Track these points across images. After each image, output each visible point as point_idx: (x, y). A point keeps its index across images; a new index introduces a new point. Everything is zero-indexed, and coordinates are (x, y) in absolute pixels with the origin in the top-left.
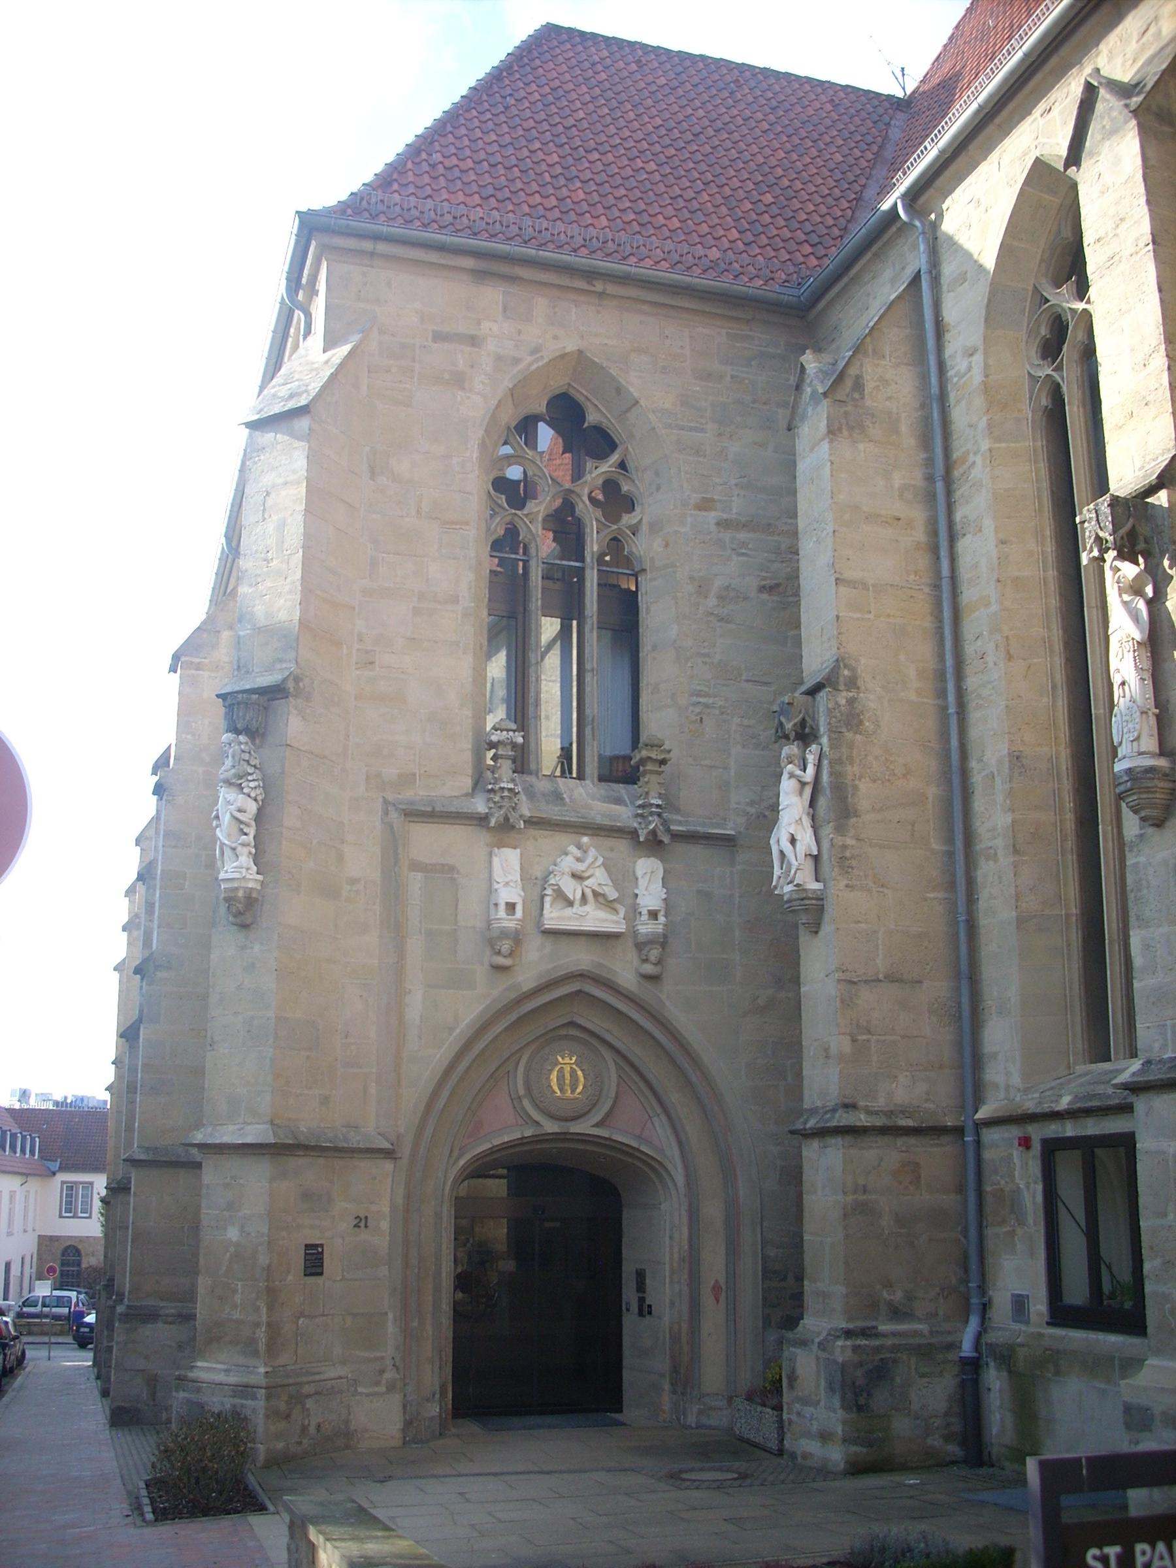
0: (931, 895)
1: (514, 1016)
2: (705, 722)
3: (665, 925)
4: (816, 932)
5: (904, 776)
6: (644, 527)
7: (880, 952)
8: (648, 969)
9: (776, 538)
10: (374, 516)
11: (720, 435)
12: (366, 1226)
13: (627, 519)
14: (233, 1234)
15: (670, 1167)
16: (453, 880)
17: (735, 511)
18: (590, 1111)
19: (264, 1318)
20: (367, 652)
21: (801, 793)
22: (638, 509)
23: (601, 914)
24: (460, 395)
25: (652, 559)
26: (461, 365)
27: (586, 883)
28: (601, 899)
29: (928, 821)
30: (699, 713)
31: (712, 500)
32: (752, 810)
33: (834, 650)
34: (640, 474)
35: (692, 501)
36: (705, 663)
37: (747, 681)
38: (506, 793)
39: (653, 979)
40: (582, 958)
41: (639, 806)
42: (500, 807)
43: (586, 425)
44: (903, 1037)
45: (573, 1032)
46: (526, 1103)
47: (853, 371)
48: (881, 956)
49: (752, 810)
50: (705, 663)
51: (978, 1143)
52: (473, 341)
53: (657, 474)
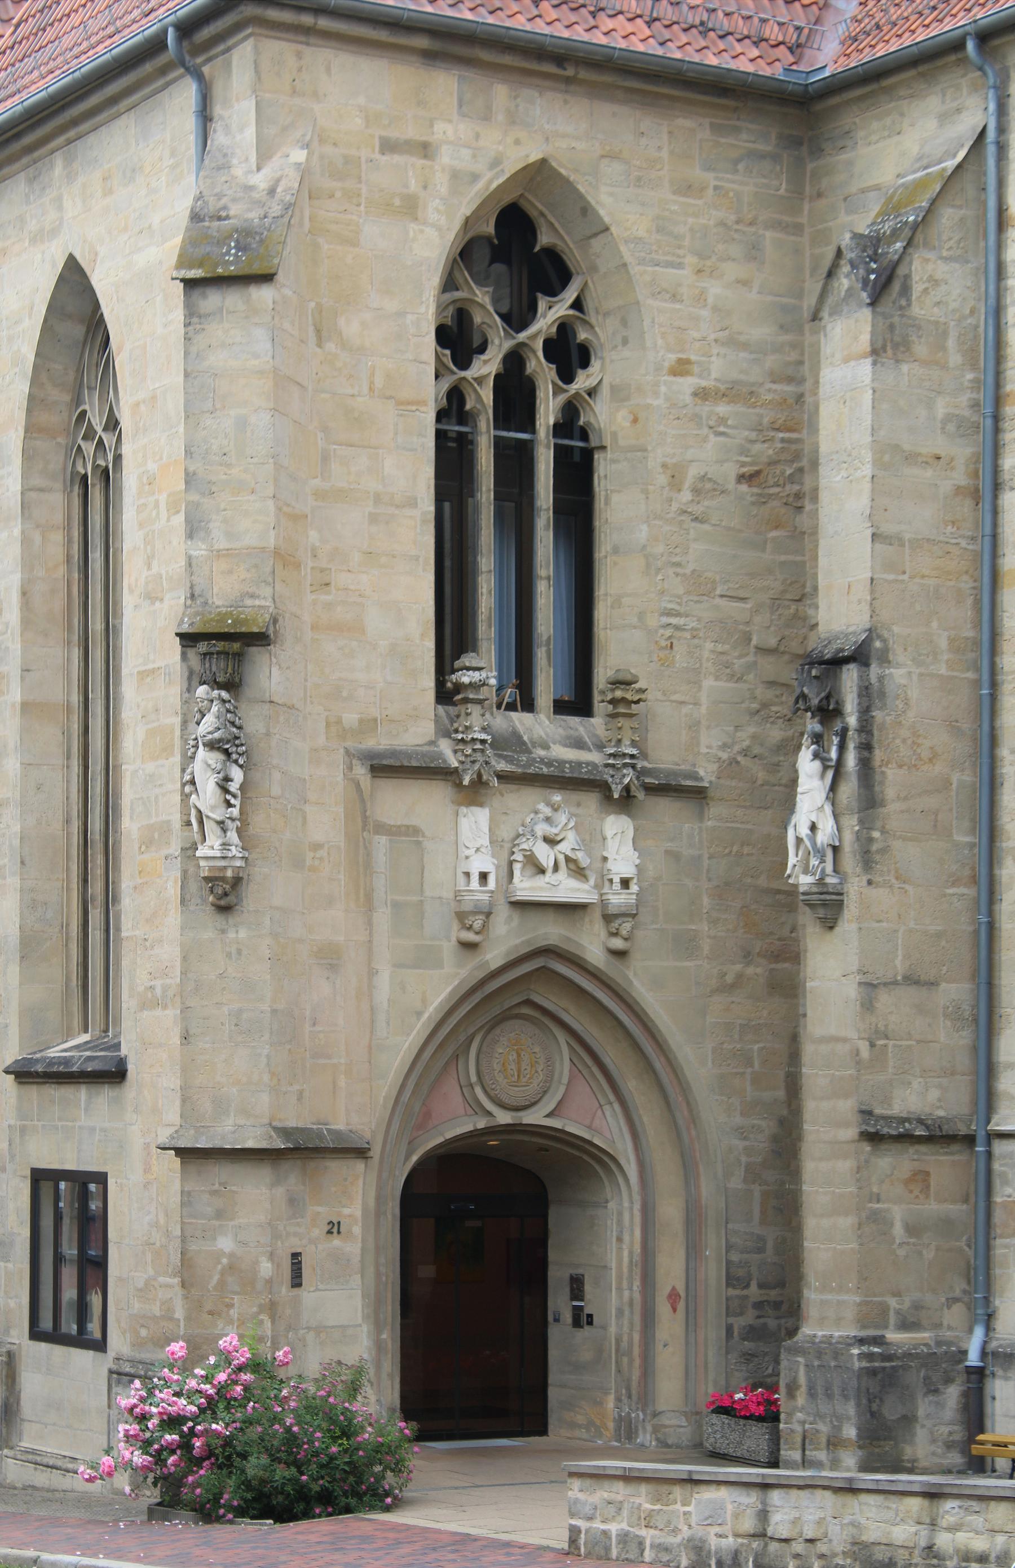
0: (950, 891)
1: (478, 997)
2: (675, 648)
3: (637, 895)
4: (831, 928)
5: (930, 760)
6: (605, 391)
7: (900, 952)
8: (618, 943)
9: (757, 410)
10: (323, 395)
11: (699, 271)
12: (339, 1232)
13: (583, 381)
14: (225, 1244)
15: (622, 1161)
16: (419, 843)
17: (714, 376)
18: (541, 1098)
19: (269, 1333)
20: (322, 570)
21: (822, 776)
22: (595, 365)
23: (573, 883)
24: (413, 226)
25: (614, 435)
26: (414, 186)
27: (560, 847)
28: (572, 866)
29: (951, 810)
30: (670, 637)
31: (688, 362)
32: (725, 756)
33: (866, 617)
34: (600, 318)
35: (666, 364)
36: (677, 575)
37: (722, 596)
38: (478, 746)
39: (620, 954)
40: (551, 931)
41: (611, 755)
42: (473, 762)
43: (537, 249)
44: (918, 1042)
45: (526, 1010)
46: (478, 1091)
47: (901, 271)
48: (900, 958)
49: (725, 756)
50: (677, 575)
51: (989, 1155)
52: (425, 150)
53: (624, 322)
